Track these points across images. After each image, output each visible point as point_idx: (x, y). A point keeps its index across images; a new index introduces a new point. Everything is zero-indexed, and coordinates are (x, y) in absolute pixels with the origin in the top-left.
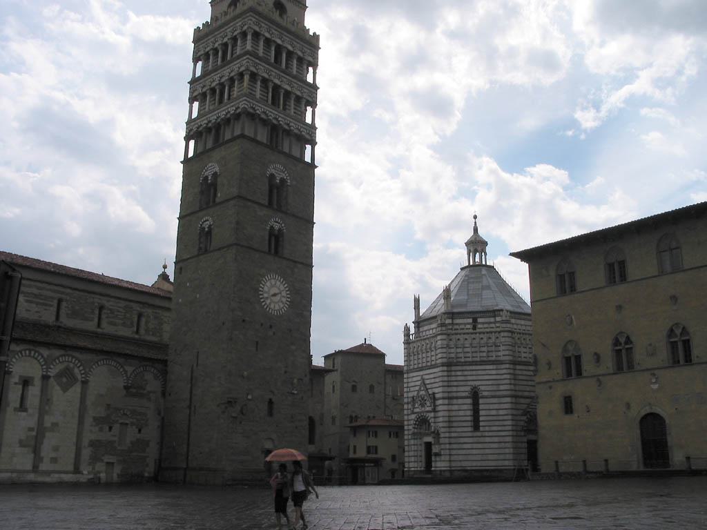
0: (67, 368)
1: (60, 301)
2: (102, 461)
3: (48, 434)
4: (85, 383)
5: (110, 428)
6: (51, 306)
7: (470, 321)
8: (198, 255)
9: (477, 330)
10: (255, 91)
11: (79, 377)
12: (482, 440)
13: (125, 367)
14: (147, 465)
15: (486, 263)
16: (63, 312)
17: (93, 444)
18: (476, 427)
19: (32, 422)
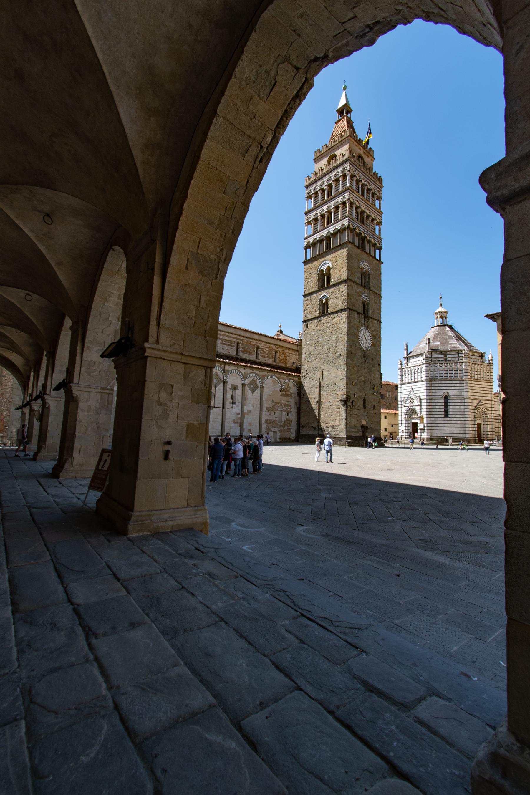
0: (253, 380)
1: (238, 344)
2: (271, 431)
3: (246, 416)
4: (262, 388)
5: (275, 413)
6: (234, 346)
7: (443, 356)
8: (319, 317)
9: (448, 362)
10: (352, 213)
11: (259, 386)
12: (450, 422)
13: (280, 380)
14: (292, 433)
15: (446, 323)
16: (240, 349)
17: (266, 422)
18: (446, 415)
19: (239, 410)
